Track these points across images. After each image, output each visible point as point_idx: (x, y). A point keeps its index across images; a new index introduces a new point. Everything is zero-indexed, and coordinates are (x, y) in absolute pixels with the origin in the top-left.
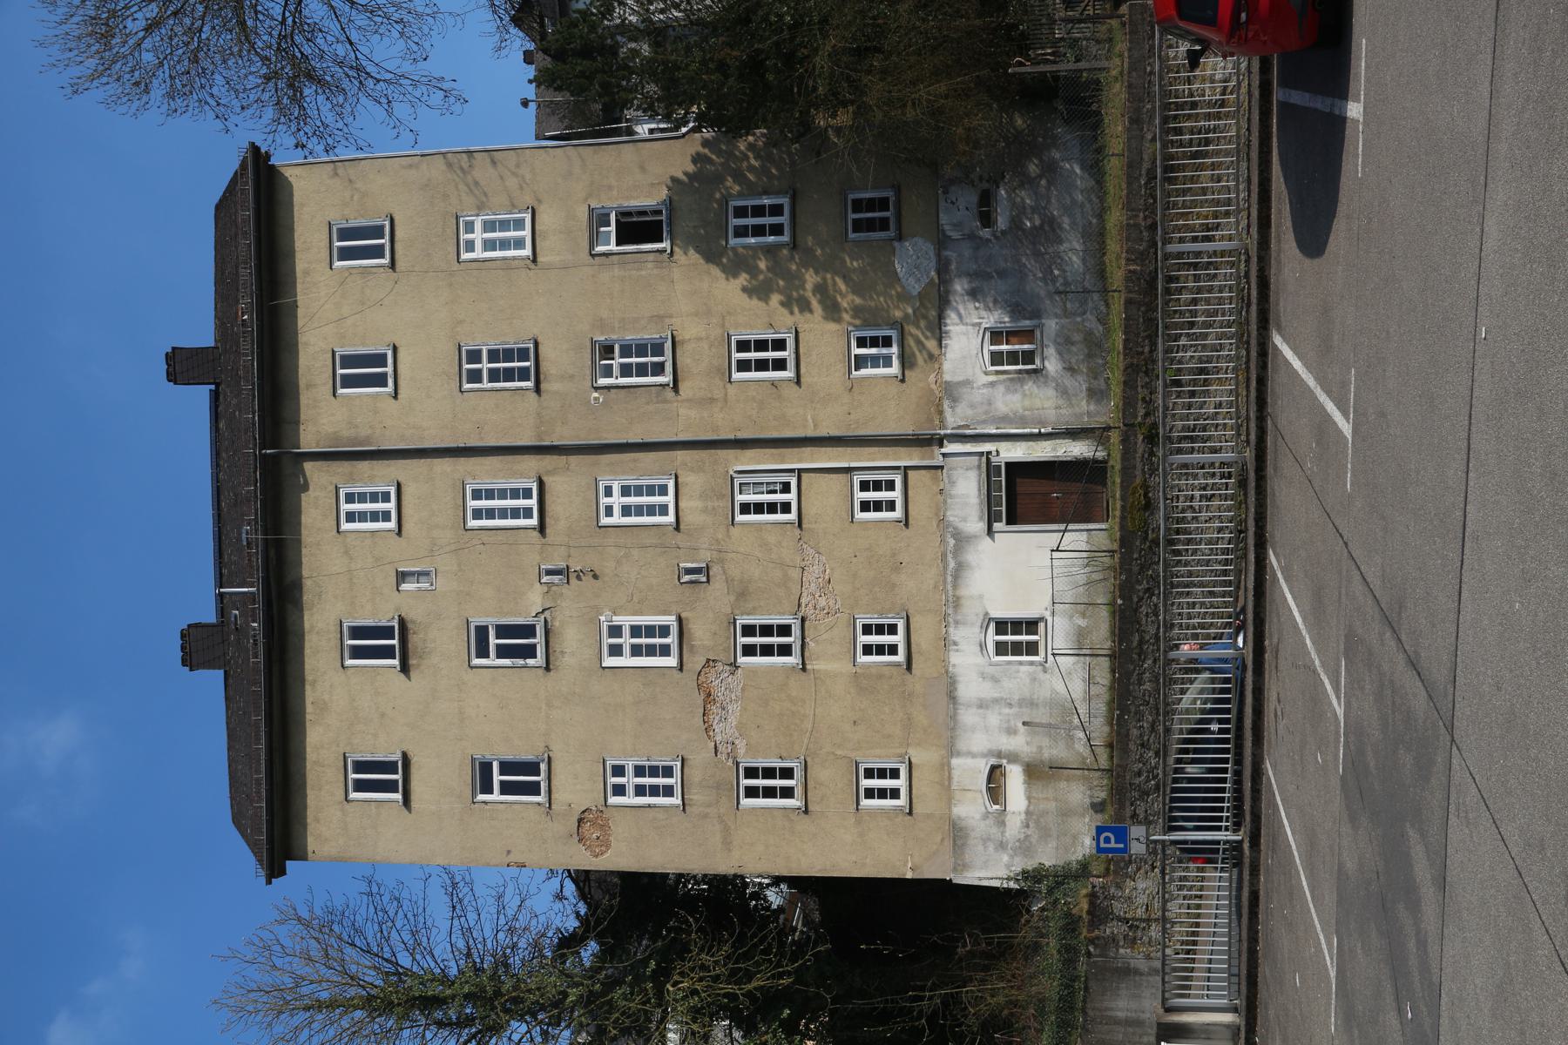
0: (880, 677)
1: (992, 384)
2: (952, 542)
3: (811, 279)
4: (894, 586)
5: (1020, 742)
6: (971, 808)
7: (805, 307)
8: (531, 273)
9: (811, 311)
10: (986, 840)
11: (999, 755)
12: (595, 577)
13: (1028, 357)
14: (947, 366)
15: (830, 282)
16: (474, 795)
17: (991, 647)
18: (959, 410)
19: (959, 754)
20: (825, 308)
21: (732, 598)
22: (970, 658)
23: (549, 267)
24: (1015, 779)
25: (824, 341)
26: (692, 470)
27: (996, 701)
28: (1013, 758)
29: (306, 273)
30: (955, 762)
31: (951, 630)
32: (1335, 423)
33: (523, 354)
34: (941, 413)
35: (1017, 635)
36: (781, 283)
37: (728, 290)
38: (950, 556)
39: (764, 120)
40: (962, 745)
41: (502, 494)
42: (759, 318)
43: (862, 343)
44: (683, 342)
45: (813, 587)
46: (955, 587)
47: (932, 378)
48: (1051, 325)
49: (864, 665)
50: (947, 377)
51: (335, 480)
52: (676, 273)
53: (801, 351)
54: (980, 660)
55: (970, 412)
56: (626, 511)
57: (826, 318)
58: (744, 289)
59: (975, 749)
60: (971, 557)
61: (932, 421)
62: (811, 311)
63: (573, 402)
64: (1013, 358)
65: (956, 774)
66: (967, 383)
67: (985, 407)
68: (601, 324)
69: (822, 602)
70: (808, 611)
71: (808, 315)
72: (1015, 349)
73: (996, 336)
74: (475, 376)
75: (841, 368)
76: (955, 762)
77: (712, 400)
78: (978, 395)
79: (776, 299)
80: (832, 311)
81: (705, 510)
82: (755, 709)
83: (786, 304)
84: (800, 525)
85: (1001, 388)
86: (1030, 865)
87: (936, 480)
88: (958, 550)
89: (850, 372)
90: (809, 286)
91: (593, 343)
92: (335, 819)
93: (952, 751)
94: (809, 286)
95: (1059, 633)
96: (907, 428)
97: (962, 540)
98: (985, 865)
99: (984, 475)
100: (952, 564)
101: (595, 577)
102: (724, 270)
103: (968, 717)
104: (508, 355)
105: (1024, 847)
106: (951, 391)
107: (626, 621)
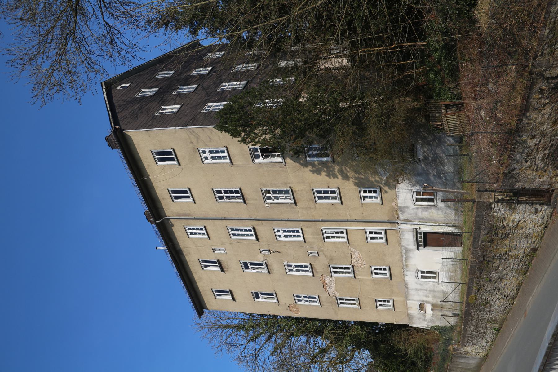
0: (381, 281)
1: (417, 208)
2: (404, 251)
3: (337, 168)
4: (384, 259)
5: (430, 299)
6: (414, 311)
7: (335, 176)
8: (232, 168)
9: (337, 178)
10: (419, 319)
11: (423, 301)
12: (279, 252)
13: (431, 200)
14: (399, 201)
15: (344, 169)
16: (254, 300)
17: (419, 277)
18: (404, 215)
19: (409, 300)
20: (342, 175)
21: (328, 260)
22: (411, 280)
23: (238, 166)
24: (428, 307)
25: (349, 188)
26: (307, 227)
27: (421, 289)
28: (428, 302)
29: (149, 166)
30: (408, 301)
31: (405, 272)
32: (545, 333)
33: (237, 192)
34: (398, 214)
35: (427, 274)
36: (325, 169)
37: (307, 173)
38: (404, 254)
39: (282, 76)
40: (410, 298)
41: (241, 230)
42: (322, 181)
43: (365, 192)
44: (296, 191)
45: (356, 258)
46: (406, 262)
47: (393, 204)
48: (440, 195)
49: (375, 278)
50: (399, 205)
51: (183, 225)
52: (288, 169)
53: (342, 195)
54: (416, 280)
55: (409, 216)
56: (286, 236)
57: (343, 179)
58: (310, 171)
59: (415, 299)
60: (411, 254)
61: (394, 216)
62: (337, 178)
63: (256, 206)
64: (425, 200)
65: (409, 304)
66: (407, 207)
67: (415, 215)
68: (264, 185)
69: (359, 262)
70: (355, 264)
71: (336, 179)
72: (426, 196)
73: (418, 193)
74: (221, 198)
75: (358, 200)
76: (408, 301)
77: (310, 208)
78: (412, 211)
79: (323, 174)
80: (346, 177)
81: (314, 238)
82: (336, 284)
83: (328, 176)
84: (348, 243)
85: (420, 210)
86: (434, 325)
87: (397, 233)
88: (406, 253)
89: (361, 201)
90: (336, 170)
91: (262, 191)
92: (212, 303)
93: (407, 299)
94: (336, 170)
95: (443, 277)
96: (386, 219)
97: (407, 251)
98: (419, 323)
99: (415, 234)
100: (404, 256)
101: (279, 252)
102: (302, 164)
103: (411, 292)
104: (231, 192)
105: (432, 321)
106: (402, 209)
107: (293, 264)
